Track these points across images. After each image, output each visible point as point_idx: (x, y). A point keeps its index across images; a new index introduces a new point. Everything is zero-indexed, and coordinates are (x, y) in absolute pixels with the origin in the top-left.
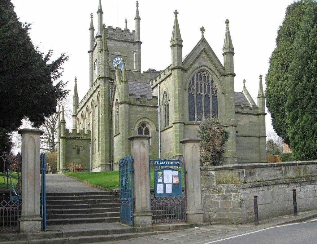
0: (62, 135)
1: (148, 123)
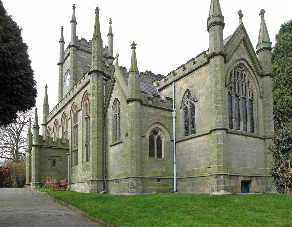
0: (34, 143)
1: (161, 130)
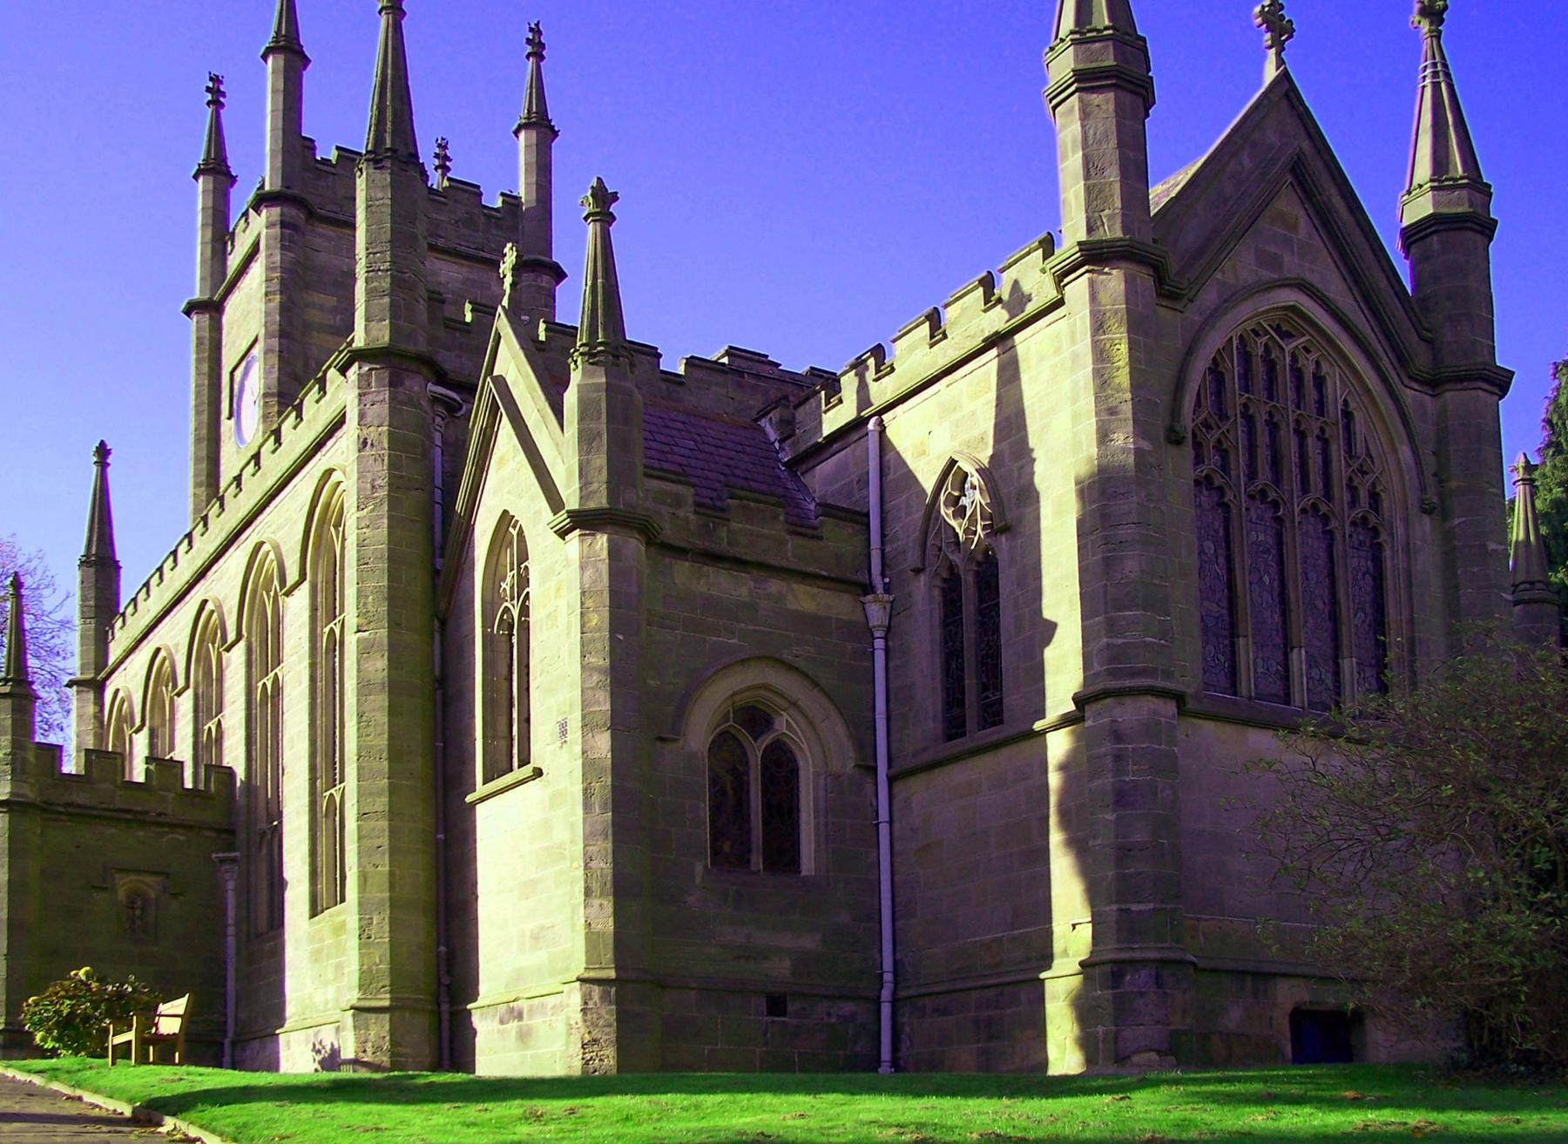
1: (794, 704)
